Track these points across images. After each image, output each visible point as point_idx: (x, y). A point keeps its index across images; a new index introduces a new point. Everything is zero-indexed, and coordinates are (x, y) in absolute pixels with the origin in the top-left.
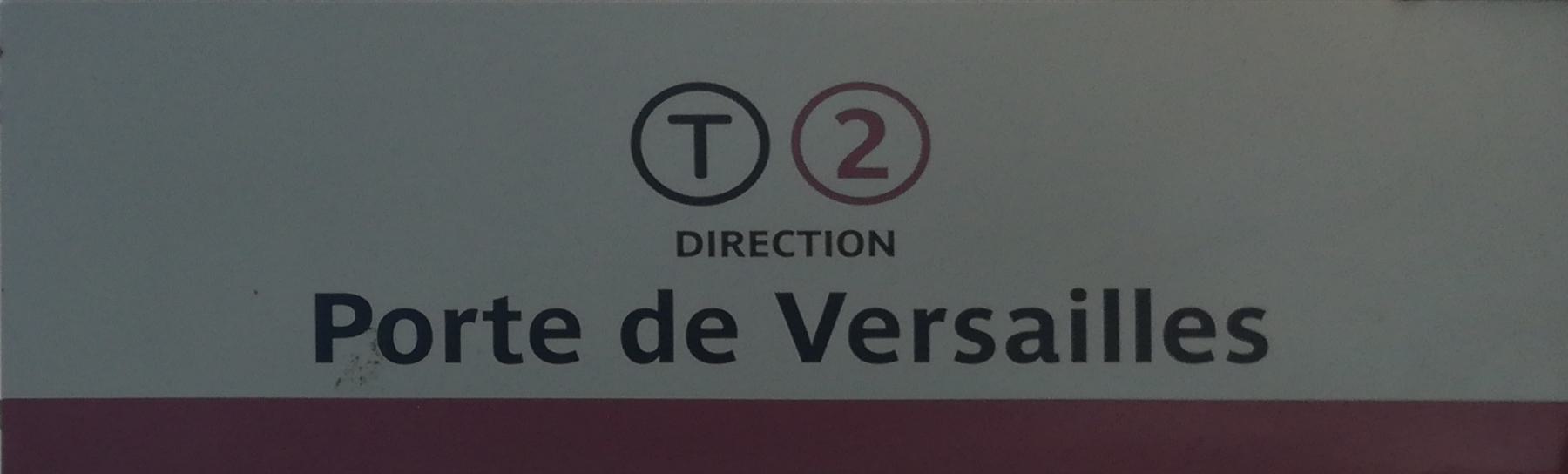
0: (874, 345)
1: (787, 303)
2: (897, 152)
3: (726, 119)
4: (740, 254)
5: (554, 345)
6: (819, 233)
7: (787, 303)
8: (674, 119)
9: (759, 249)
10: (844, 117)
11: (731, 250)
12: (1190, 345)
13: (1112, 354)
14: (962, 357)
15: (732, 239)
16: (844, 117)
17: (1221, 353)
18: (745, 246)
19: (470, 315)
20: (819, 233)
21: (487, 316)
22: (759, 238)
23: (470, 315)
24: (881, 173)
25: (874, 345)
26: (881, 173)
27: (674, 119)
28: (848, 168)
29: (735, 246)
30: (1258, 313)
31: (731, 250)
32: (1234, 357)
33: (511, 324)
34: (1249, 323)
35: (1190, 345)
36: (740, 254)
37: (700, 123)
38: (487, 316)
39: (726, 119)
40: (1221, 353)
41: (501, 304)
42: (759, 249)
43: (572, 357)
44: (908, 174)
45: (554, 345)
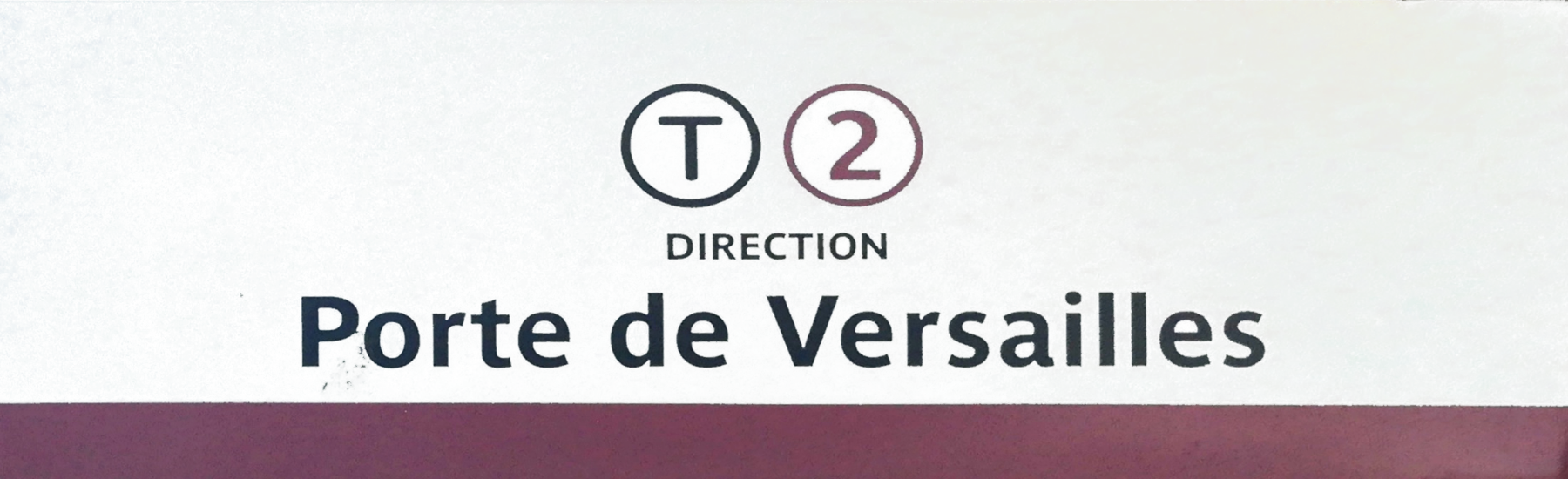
0: (866, 349)
2: (890, 155)
3: (716, 121)
4: (731, 256)
6: (811, 236)
8: (665, 121)
9: (750, 251)
10: (836, 119)
11: (721, 252)
13: (1107, 357)
15: (723, 241)
16: (836, 119)
18: (736, 249)
19: (458, 319)
20: (811, 236)
22: (750, 241)
24: (874, 175)
25: (866, 349)
26: (874, 175)
27: (665, 121)
28: (841, 171)
29: (726, 248)
31: (721, 252)
36: (731, 256)
37: (691, 125)
39: (716, 121)
41: (489, 307)
42: (750, 251)
45: (541, 348)
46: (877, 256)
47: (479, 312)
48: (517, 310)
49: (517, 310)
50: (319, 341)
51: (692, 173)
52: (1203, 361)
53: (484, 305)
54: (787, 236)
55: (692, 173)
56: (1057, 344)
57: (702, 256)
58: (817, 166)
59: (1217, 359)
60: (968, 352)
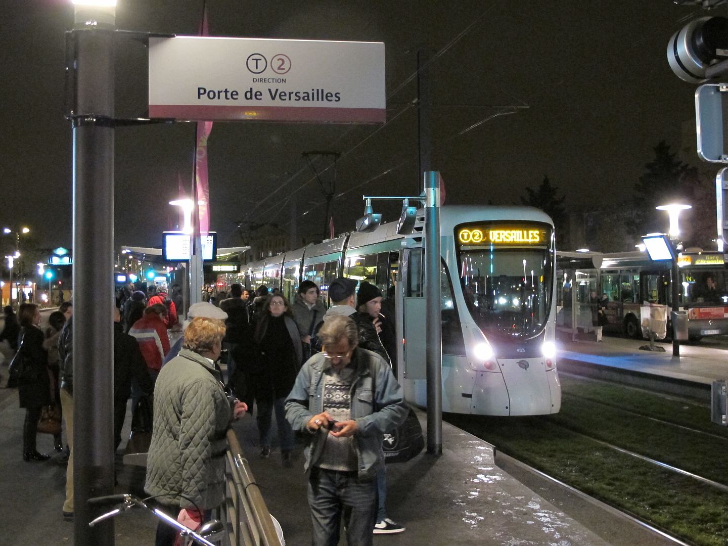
0: (283, 97)
2: (286, 66)
3: (260, 60)
12: (329, 98)
13: (318, 100)
19: (222, 91)
24: (284, 69)
25: (283, 97)
26: (284, 69)
27: (253, 59)
28: (279, 68)
30: (339, 93)
34: (337, 95)
37: (257, 60)
39: (260, 60)
51: (257, 68)
55: (257, 68)
58: (275, 67)
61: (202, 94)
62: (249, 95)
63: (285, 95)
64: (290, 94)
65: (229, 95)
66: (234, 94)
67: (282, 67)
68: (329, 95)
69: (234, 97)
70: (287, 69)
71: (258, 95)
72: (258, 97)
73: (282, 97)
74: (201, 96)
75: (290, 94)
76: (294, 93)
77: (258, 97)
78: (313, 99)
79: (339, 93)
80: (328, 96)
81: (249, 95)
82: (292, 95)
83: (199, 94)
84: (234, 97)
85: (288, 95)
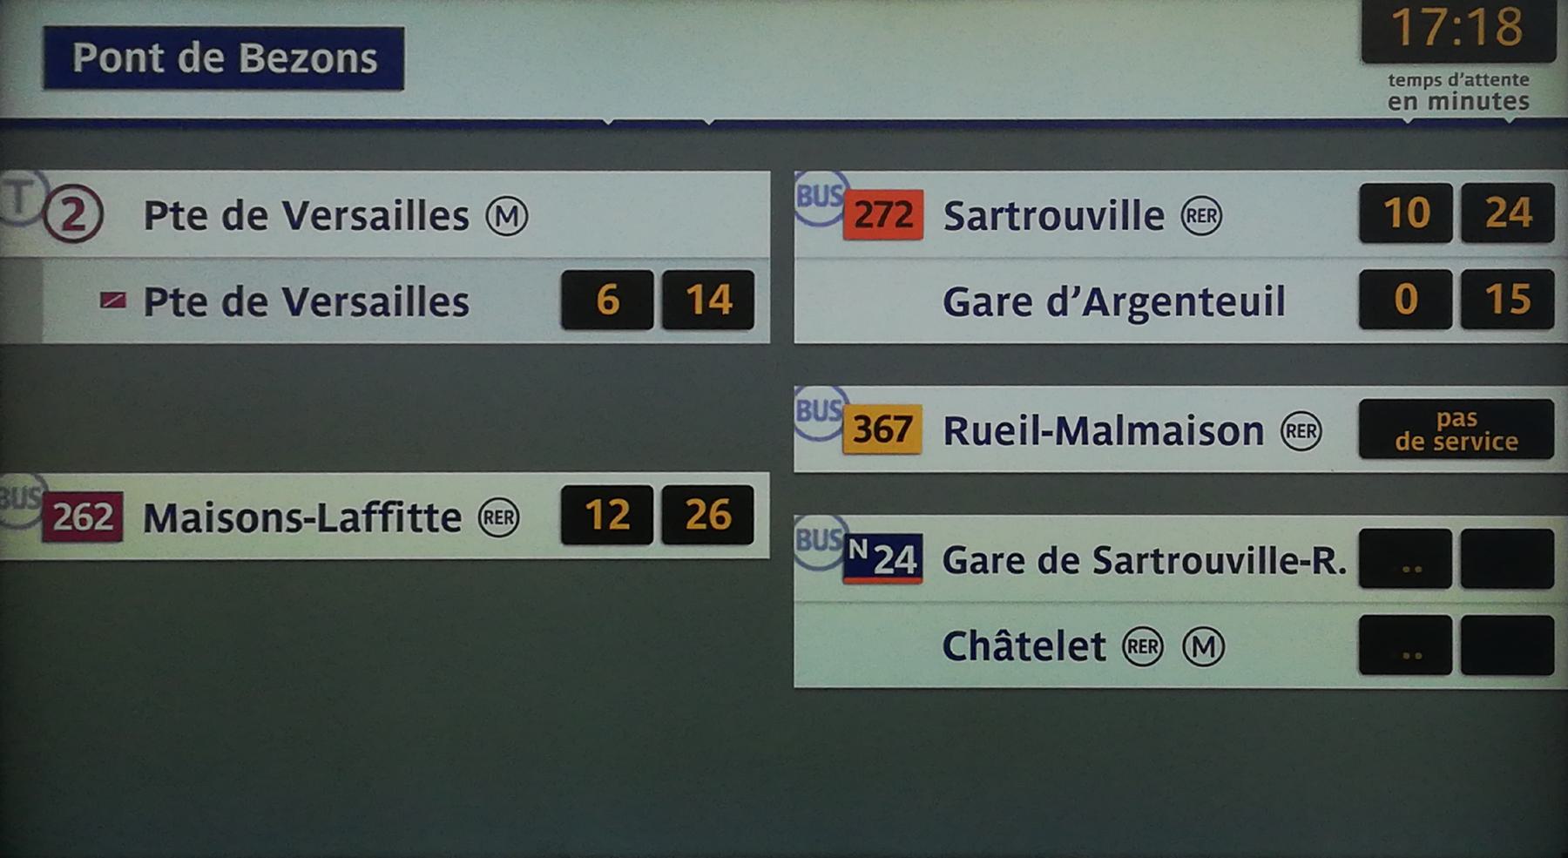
0: (321, 222)
1: (286, 291)
2: (88, 218)
4: (964, 442)
5: (197, 222)
6: (963, 634)
7: (286, 291)
12: (440, 309)
14: (354, 228)
15: (956, 425)
17: (451, 313)
19: (1001, 210)
20: (963, 634)
21: (1152, 556)
23: (1001, 210)
24: (82, 228)
25: (321, 222)
26: (82, 228)
28: (68, 226)
29: (958, 432)
31: (954, 436)
32: (456, 314)
33: (1210, 299)
35: (440, 309)
36: (964, 442)
38: (1152, 556)
40: (451, 313)
41: (431, 507)
43: (264, 314)
44: (806, 562)
45: (197, 222)
46: (504, 209)
47: (427, 509)
48: (187, 206)
49: (187, 206)
50: (200, 41)
52: (446, 228)
53: (1088, 314)
54: (892, 418)
56: (392, 222)
57: (988, 426)
59: (451, 227)
60: (359, 224)
61: (157, 217)
62: (1048, 563)
63: (328, 217)
64: (340, 212)
65: (1489, 81)
66: (1022, 304)
67: (77, 222)
68: (1070, 559)
69: (197, 309)
70: (89, 228)
71: (257, 304)
72: (1154, 222)
73: (1152, 221)
74: (155, 221)
75: (340, 212)
76: (350, 211)
77: (1154, 222)
78: (398, 227)
79: (465, 210)
80: (437, 304)
81: (1048, 563)
82: (1000, 560)
83: (150, 218)
84: (197, 309)
85: (1501, 80)
